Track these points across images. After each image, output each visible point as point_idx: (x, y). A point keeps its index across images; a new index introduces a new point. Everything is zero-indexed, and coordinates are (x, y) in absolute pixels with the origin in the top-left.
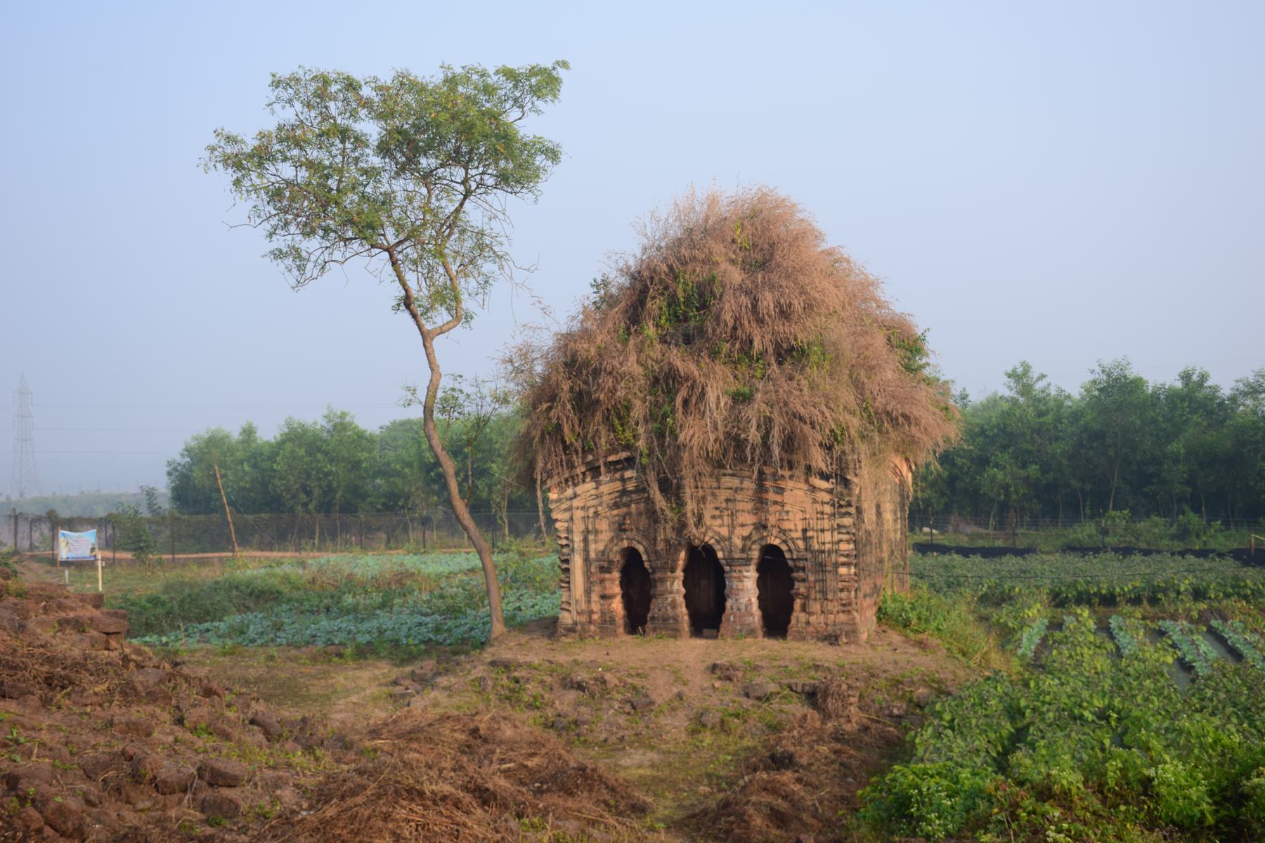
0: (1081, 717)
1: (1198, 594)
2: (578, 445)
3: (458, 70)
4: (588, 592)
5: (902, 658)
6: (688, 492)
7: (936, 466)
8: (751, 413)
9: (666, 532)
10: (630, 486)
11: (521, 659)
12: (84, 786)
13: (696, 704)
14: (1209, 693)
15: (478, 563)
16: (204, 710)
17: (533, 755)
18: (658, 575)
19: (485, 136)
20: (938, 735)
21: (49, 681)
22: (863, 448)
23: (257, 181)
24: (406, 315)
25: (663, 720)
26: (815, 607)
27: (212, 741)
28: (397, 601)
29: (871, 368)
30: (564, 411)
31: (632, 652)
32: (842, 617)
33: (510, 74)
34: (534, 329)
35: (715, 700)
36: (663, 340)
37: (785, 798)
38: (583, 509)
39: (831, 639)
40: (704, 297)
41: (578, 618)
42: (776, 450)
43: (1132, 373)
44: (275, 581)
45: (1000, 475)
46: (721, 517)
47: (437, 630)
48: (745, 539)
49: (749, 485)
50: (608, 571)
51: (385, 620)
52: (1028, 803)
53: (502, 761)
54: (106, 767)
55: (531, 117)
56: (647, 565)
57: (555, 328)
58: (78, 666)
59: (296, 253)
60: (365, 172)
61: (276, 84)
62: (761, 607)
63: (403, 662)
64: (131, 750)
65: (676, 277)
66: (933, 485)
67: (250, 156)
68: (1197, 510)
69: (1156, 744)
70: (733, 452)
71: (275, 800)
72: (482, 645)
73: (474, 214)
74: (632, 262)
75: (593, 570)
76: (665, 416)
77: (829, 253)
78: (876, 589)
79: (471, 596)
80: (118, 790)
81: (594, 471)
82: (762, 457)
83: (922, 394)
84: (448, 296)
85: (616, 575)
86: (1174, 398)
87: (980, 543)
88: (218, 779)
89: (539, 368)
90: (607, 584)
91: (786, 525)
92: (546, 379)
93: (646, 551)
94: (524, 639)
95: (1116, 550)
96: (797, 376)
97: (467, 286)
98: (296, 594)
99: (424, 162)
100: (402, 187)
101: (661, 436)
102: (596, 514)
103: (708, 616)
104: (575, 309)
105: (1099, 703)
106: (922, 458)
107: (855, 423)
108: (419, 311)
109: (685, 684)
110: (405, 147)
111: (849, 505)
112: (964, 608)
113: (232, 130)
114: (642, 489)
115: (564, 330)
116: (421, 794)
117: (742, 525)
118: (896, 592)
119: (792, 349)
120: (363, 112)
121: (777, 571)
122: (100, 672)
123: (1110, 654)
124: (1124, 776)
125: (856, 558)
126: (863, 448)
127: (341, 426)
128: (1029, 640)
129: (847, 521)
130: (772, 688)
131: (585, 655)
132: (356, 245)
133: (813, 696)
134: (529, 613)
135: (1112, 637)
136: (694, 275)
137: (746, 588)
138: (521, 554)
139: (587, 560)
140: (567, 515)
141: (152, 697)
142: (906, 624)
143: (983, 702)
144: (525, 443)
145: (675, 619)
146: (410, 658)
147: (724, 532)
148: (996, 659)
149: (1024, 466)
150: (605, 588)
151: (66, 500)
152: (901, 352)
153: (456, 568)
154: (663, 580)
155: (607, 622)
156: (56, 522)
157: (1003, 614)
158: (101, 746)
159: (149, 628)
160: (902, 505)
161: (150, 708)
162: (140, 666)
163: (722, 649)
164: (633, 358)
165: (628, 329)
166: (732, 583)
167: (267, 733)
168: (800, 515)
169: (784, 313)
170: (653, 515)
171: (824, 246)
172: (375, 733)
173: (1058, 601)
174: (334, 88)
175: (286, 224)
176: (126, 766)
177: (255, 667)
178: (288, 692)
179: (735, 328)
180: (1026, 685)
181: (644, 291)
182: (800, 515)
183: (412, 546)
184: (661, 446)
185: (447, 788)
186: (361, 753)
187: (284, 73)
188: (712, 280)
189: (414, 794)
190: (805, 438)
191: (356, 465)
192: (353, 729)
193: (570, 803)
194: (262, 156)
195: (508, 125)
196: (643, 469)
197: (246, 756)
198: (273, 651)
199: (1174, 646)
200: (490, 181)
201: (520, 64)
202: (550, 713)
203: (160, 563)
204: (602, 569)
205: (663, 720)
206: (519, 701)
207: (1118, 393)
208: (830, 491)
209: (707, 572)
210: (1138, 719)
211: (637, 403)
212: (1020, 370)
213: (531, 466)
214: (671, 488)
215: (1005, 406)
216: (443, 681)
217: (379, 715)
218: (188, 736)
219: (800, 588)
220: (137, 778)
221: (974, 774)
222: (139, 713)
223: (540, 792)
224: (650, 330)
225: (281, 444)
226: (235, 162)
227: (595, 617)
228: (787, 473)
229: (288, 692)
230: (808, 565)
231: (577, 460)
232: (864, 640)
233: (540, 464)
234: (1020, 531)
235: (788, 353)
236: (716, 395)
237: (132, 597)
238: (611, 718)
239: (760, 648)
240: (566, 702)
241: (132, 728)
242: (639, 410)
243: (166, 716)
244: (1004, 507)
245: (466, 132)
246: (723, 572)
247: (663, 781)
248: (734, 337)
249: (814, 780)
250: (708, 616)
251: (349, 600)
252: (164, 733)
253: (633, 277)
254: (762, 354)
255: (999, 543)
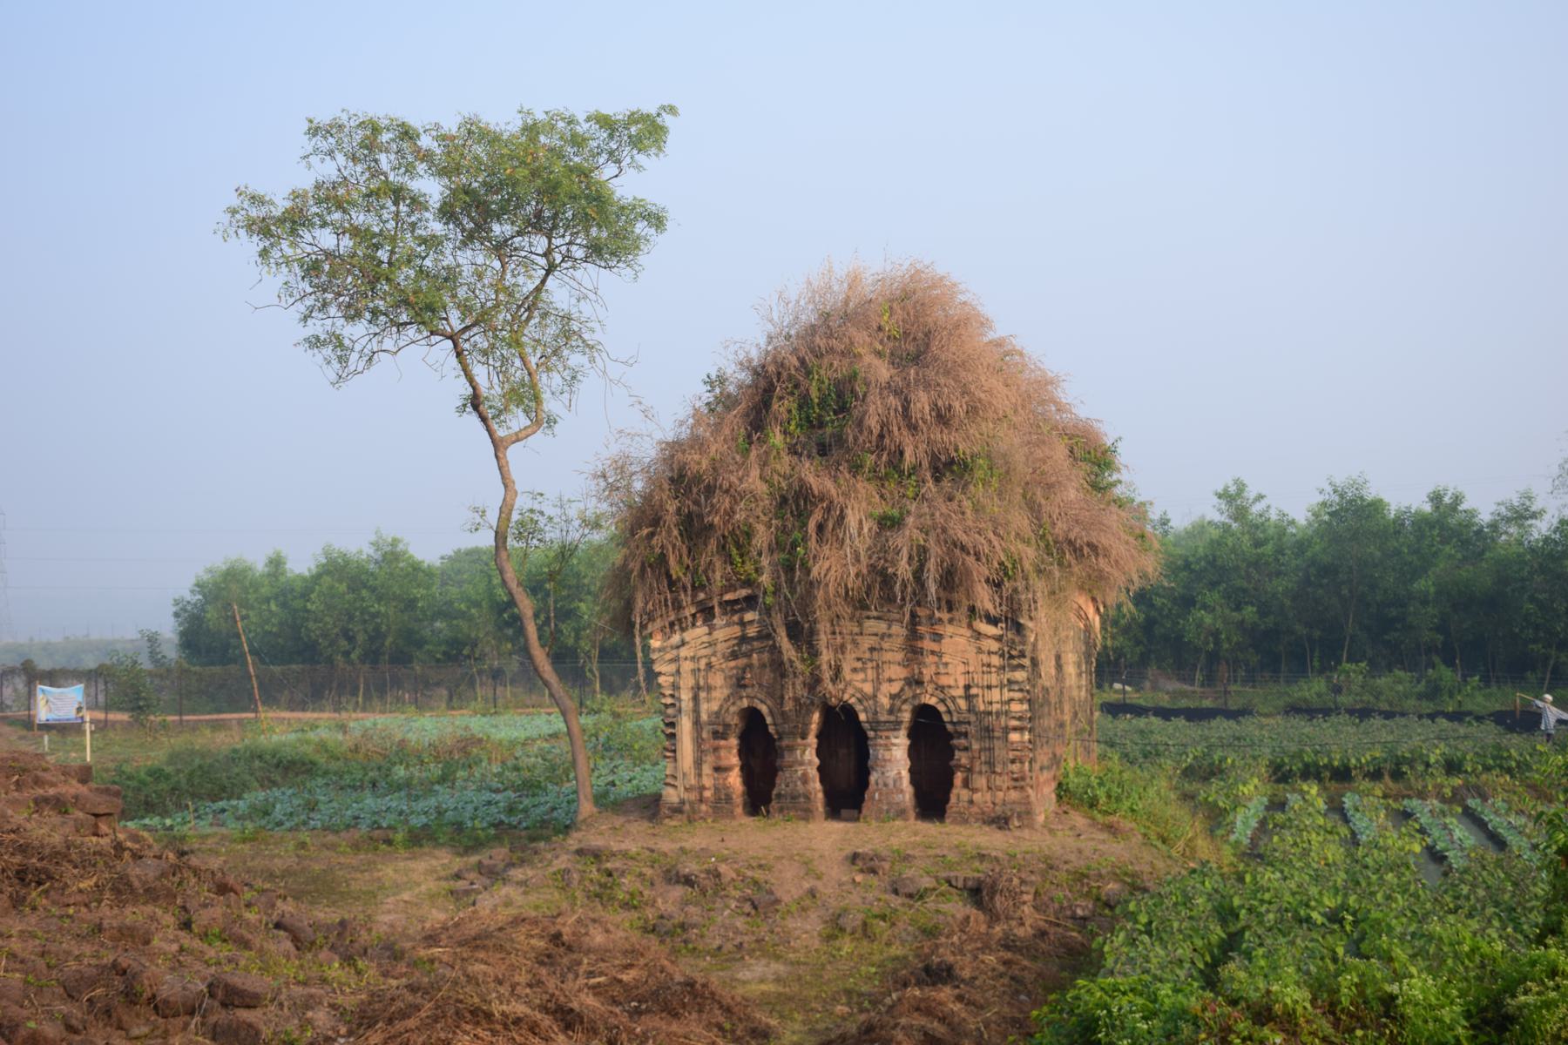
0: (1308, 919)
1: (1452, 767)
2: (687, 580)
3: (540, 116)
4: (698, 763)
5: (1088, 847)
6: (823, 639)
7: (1129, 607)
8: (903, 541)
9: (795, 689)
10: (752, 631)
11: (615, 846)
12: (62, 1007)
13: (833, 903)
14: (1465, 889)
15: (562, 726)
16: (218, 911)
17: (630, 966)
18: (785, 742)
19: (573, 198)
20: (1132, 942)
21: (21, 875)
22: (1039, 585)
23: (289, 251)
24: (474, 419)
25: (790, 923)
26: (980, 781)
27: (226, 950)
28: (461, 774)
29: (1050, 486)
30: (669, 538)
31: (753, 838)
32: (1014, 795)
33: (605, 122)
34: (632, 436)
35: (855, 898)
36: (793, 451)
37: (942, 1020)
38: (692, 660)
39: (1000, 822)
40: (843, 397)
41: (686, 796)
42: (932, 588)
43: (1371, 494)
44: (308, 749)
45: (1208, 619)
46: (863, 670)
47: (511, 810)
48: (893, 697)
49: (899, 631)
50: (724, 736)
51: (445, 797)
52: (1243, 1026)
53: (590, 974)
54: (92, 983)
55: (630, 175)
56: (771, 729)
57: (658, 436)
58: (59, 856)
59: (337, 341)
60: (423, 241)
61: (314, 131)
62: (913, 782)
63: (468, 851)
64: (124, 962)
65: (808, 373)
66: (1126, 630)
67: (281, 221)
68: (1449, 662)
69: (1400, 953)
70: (879, 590)
71: (306, 1024)
72: (567, 829)
73: (559, 293)
74: (754, 354)
75: (705, 735)
76: (794, 545)
77: (999, 344)
78: (1056, 760)
79: (553, 768)
80: (108, 1013)
81: (707, 613)
82: (914, 596)
83: (1113, 518)
84: (526, 395)
85: (734, 741)
86: (1422, 524)
87: (1184, 703)
88: (233, 997)
89: (638, 485)
90: (723, 753)
91: (944, 681)
92: (647, 498)
93: (771, 713)
94: (619, 821)
95: (1351, 712)
96: (959, 496)
97: (549, 383)
98: (334, 766)
99: (497, 228)
100: (469, 260)
101: (789, 569)
102: (709, 666)
103: (847, 793)
104: (684, 412)
105: (1330, 902)
106: (1112, 598)
107: (1030, 554)
108: (490, 414)
109: (819, 878)
110: (473, 210)
111: (1022, 655)
112: (1164, 783)
113: (261, 191)
114: (766, 635)
115: (670, 437)
116: (489, 1016)
117: (890, 680)
118: (1080, 763)
119: (952, 462)
120: (421, 167)
121: (934, 738)
122: (86, 864)
123: (1343, 841)
124: (1361, 993)
125: (1030, 721)
126: (1039, 585)
127: (392, 556)
128: (1244, 823)
129: (1020, 675)
130: (927, 882)
131: (696, 842)
132: (411, 331)
133: (977, 893)
134: (625, 789)
135: (1346, 820)
136: (831, 370)
137: (894, 759)
138: (616, 715)
139: (697, 723)
140: (672, 668)
141: (151, 894)
142: (1093, 803)
143: (1187, 900)
144: (621, 577)
145: (807, 797)
146: (476, 845)
147: (868, 688)
148: (1202, 844)
149: (1238, 608)
150: (719, 758)
151: (47, 648)
152: (1087, 467)
153: (535, 734)
154: (791, 749)
155: (722, 800)
156: (34, 675)
157: (1213, 792)
158: (86, 956)
159: (149, 807)
160: (1088, 655)
161: (149, 909)
162: (137, 856)
163: (865, 834)
164: (755, 472)
165: (749, 436)
166: (877, 752)
167: (296, 940)
168: (961, 668)
169: (943, 417)
170: (779, 667)
171: (991, 336)
172: (431, 939)
173: (1280, 774)
174: (385, 137)
175: (325, 305)
176: (118, 982)
177: (282, 856)
178: (322, 887)
179: (881, 436)
180: (1241, 879)
181: (769, 390)
182: (961, 668)
183: (479, 705)
184: (790, 582)
185: (520, 1009)
186: (413, 964)
187: (324, 118)
188: (853, 377)
189: (480, 1015)
190: (968, 573)
191: (411, 604)
192: (405, 935)
193: (675, 1027)
194: (295, 220)
195: (602, 184)
196: (768, 610)
197: (269, 969)
198: (304, 836)
199: (1422, 831)
200: (579, 253)
201: (617, 108)
202: (650, 913)
203: (164, 726)
204: (717, 735)
205: (790, 923)
206: (612, 898)
207: (1353, 517)
208: (999, 639)
209: (847, 738)
210: (1378, 922)
211: (761, 528)
212: (1233, 489)
213: (629, 606)
214: (801, 634)
215: (1215, 533)
216: (517, 874)
217: (437, 916)
218: (197, 944)
219: (962, 758)
220: (131, 997)
221: (1176, 991)
222: (135, 914)
223: (637, 1012)
224: (777, 439)
225: (317, 578)
226: (262, 228)
227: (707, 794)
228: (945, 616)
229: (322, 887)
230: (972, 729)
231: (685, 599)
232: (1040, 824)
233: (639, 604)
234: (1233, 688)
235: (947, 467)
236: (859, 517)
237: (127, 768)
238: (727, 918)
239: (911, 833)
240: (670, 900)
241: (126, 934)
242: (762, 537)
243: (169, 919)
244: (1213, 658)
245: (548, 193)
246: (866, 738)
247: (790, 999)
248: (880, 448)
249: (978, 997)
250: (847, 793)
251: (400, 772)
252: (167, 940)
253: (756, 373)
254: (915, 469)
255: (1207, 703)
